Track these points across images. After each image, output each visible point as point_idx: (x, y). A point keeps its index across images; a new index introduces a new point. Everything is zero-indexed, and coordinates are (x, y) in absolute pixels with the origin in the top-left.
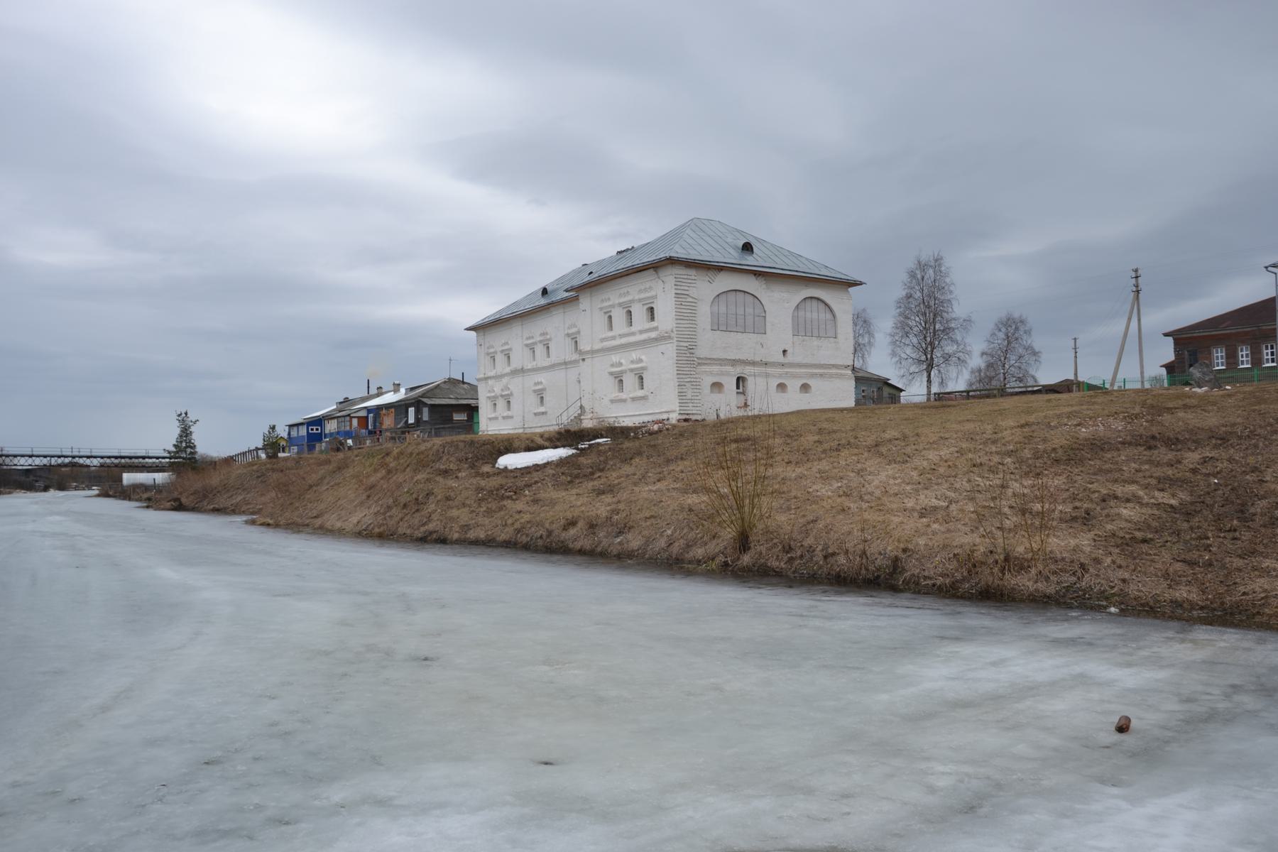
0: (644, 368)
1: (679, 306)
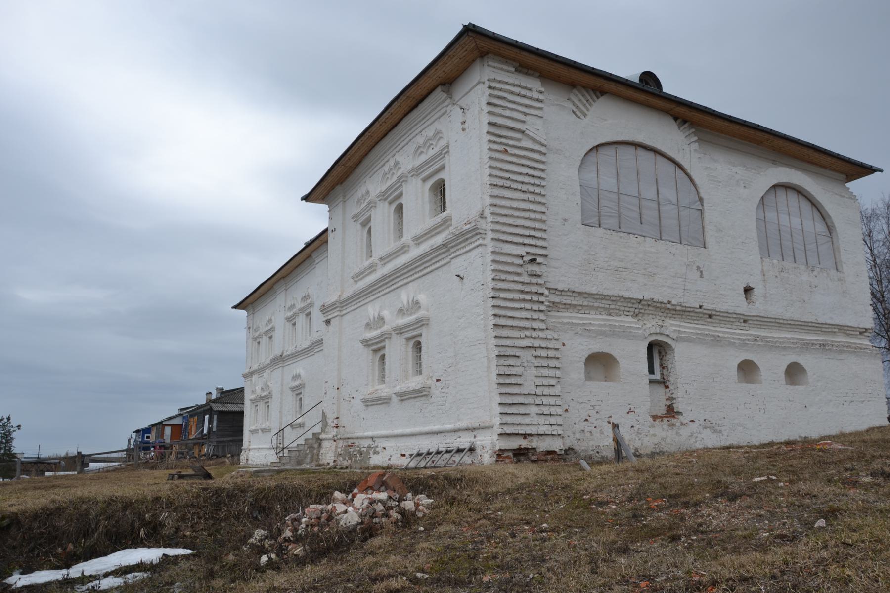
0: (422, 323)
1: (498, 155)
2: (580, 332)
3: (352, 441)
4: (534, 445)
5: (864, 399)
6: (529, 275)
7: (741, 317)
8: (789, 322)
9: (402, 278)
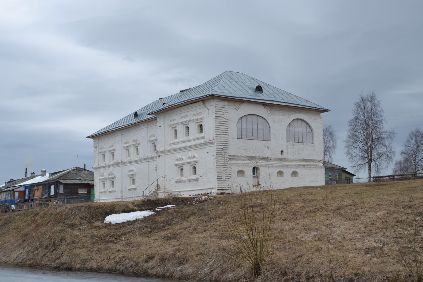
3: (171, 193)
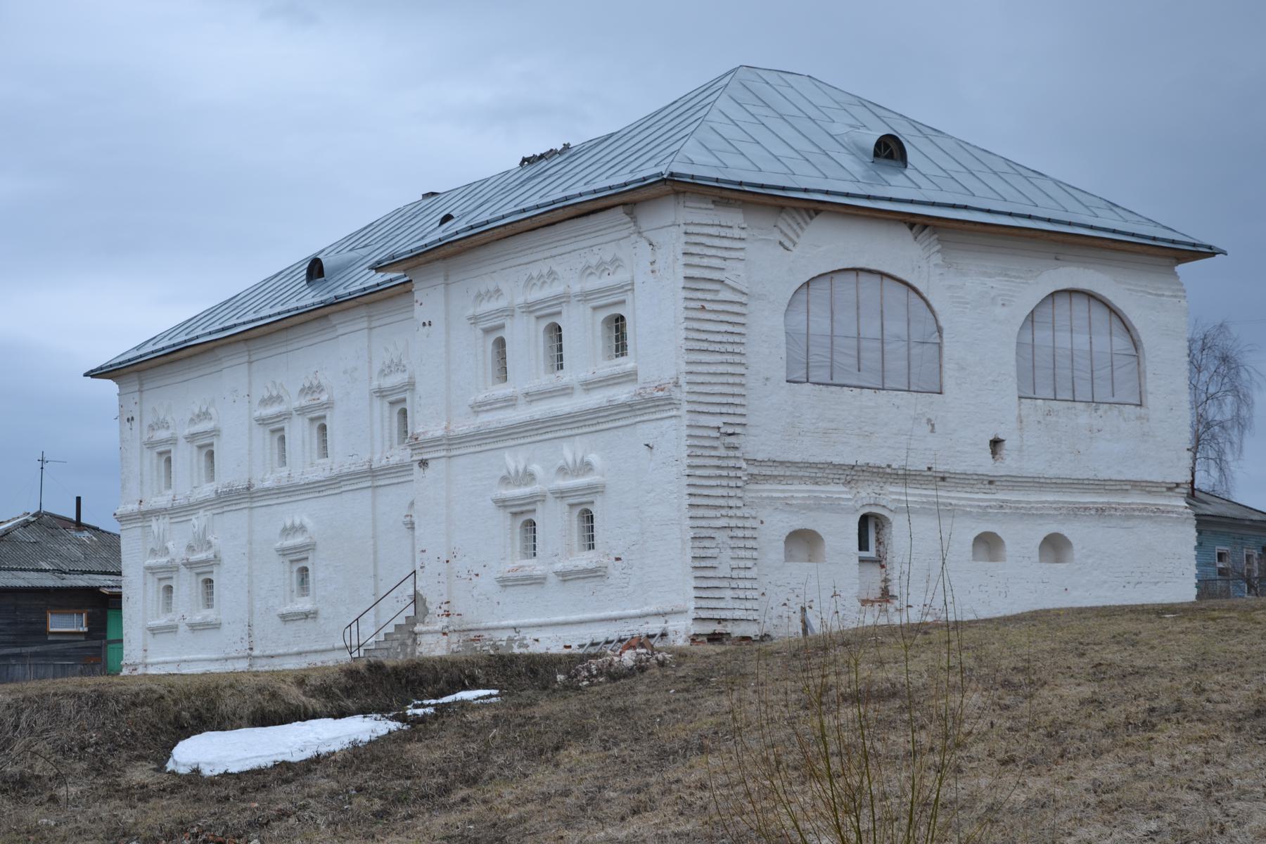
2: (781, 508)
3: (477, 633)
4: (729, 630)
5: (1157, 580)
6: (726, 447)
7: (985, 478)
8: (1054, 481)
9: (563, 427)
